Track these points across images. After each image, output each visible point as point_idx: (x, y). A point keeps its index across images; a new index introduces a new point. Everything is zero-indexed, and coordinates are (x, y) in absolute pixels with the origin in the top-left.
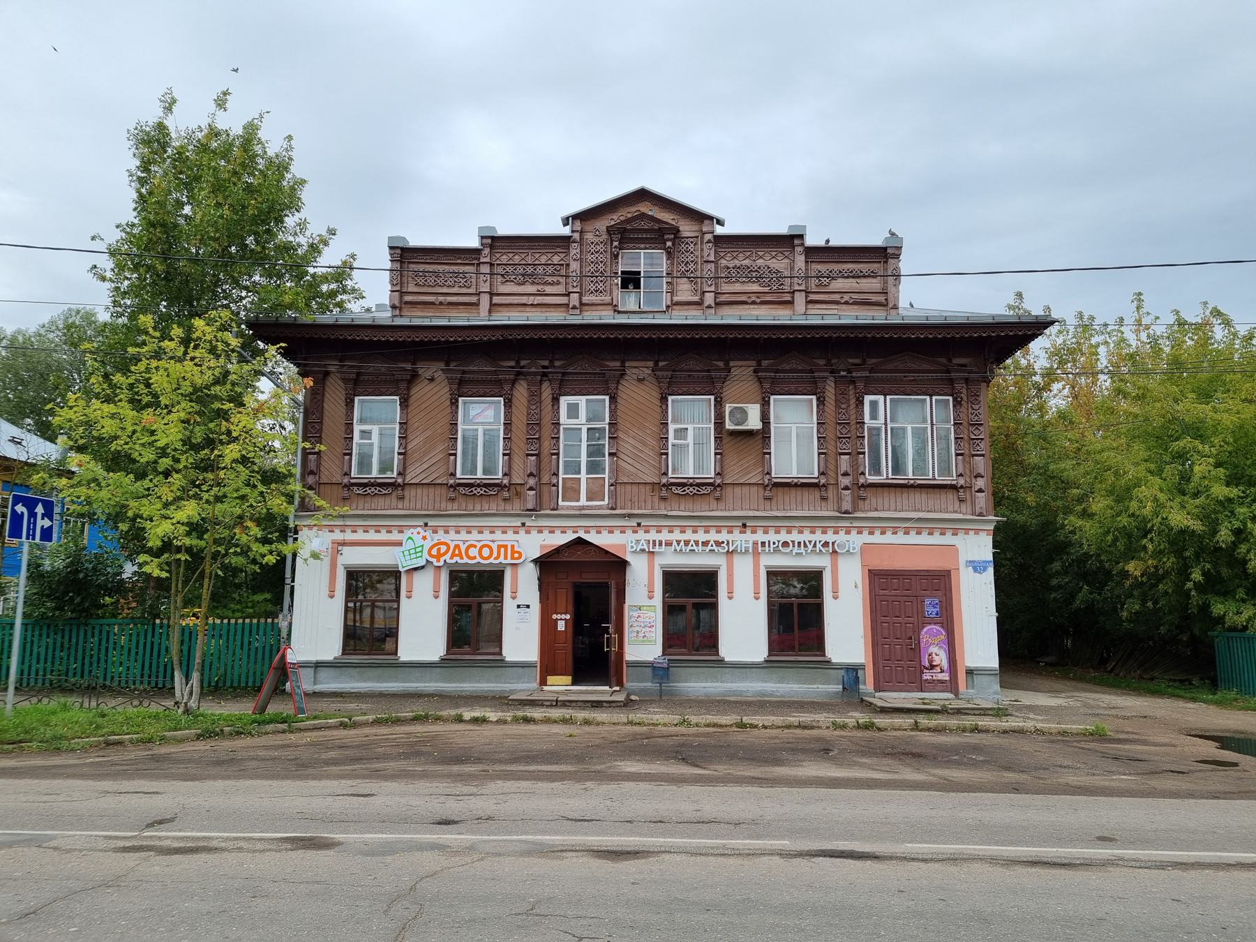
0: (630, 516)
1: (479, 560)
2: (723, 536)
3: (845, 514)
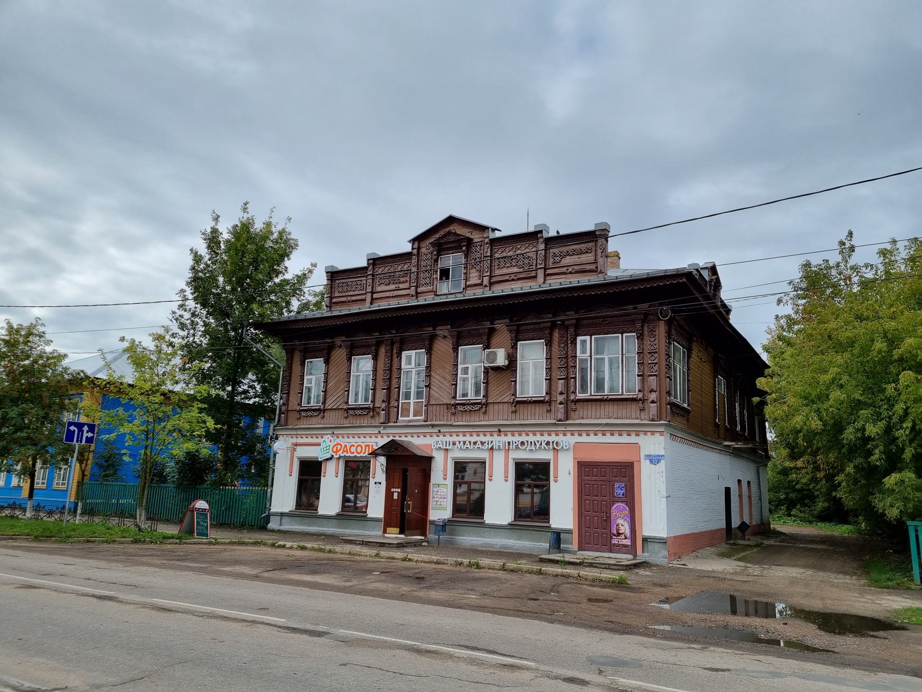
0: (433, 426)
1: (355, 454)
2: (488, 438)
3: (560, 422)
